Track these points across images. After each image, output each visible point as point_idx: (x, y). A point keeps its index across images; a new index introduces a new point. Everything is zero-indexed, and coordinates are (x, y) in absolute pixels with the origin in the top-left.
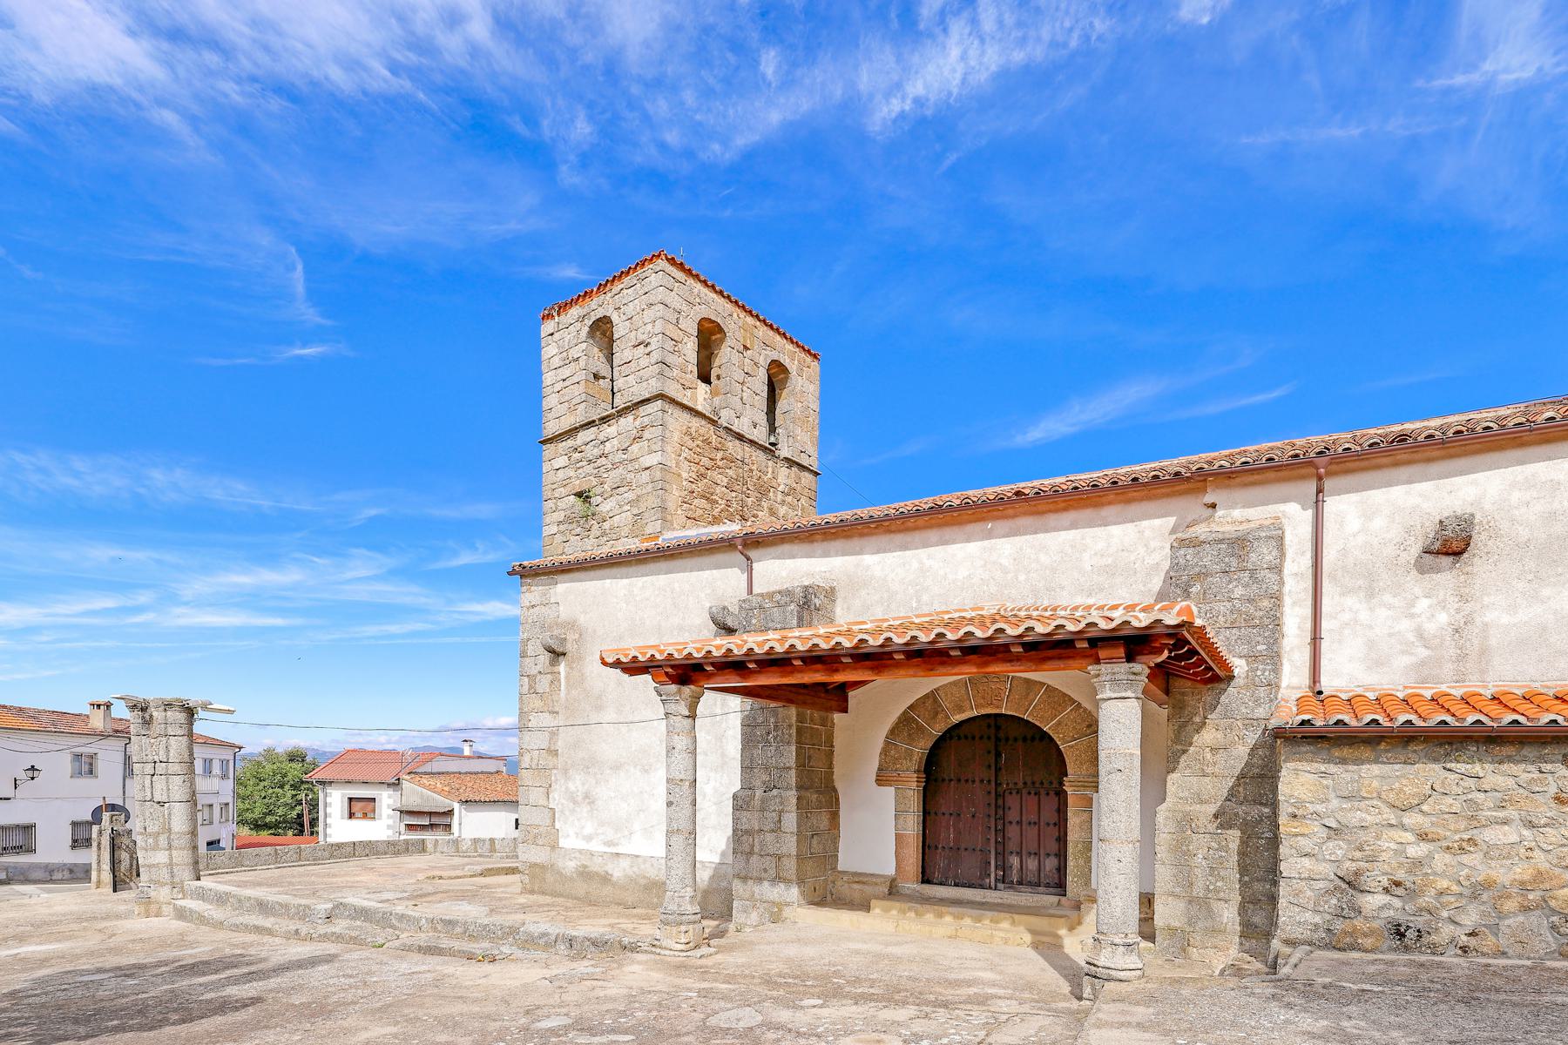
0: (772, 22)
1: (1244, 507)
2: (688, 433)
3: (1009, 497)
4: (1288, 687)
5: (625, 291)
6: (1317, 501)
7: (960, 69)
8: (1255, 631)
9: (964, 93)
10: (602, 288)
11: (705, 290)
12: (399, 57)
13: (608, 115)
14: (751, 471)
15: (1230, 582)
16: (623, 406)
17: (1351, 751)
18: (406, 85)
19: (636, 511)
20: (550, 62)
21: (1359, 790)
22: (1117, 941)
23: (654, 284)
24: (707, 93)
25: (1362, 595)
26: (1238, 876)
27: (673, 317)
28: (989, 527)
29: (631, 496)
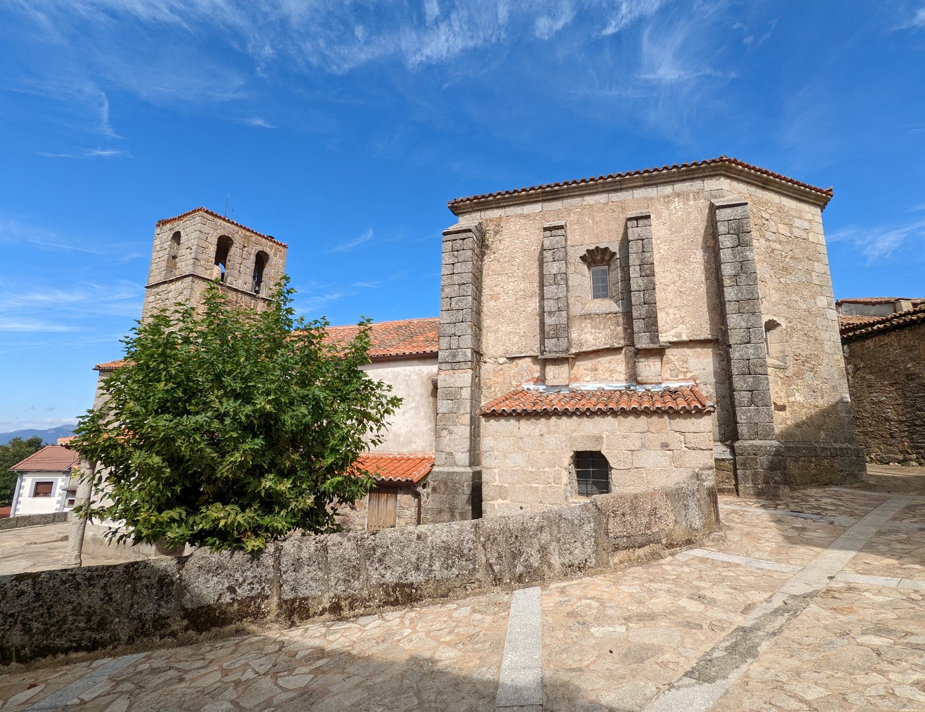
0: (360, 11)
7: (446, 45)
10: (180, 218)
18: (177, 18)
20: (254, 20)
24: (330, 42)
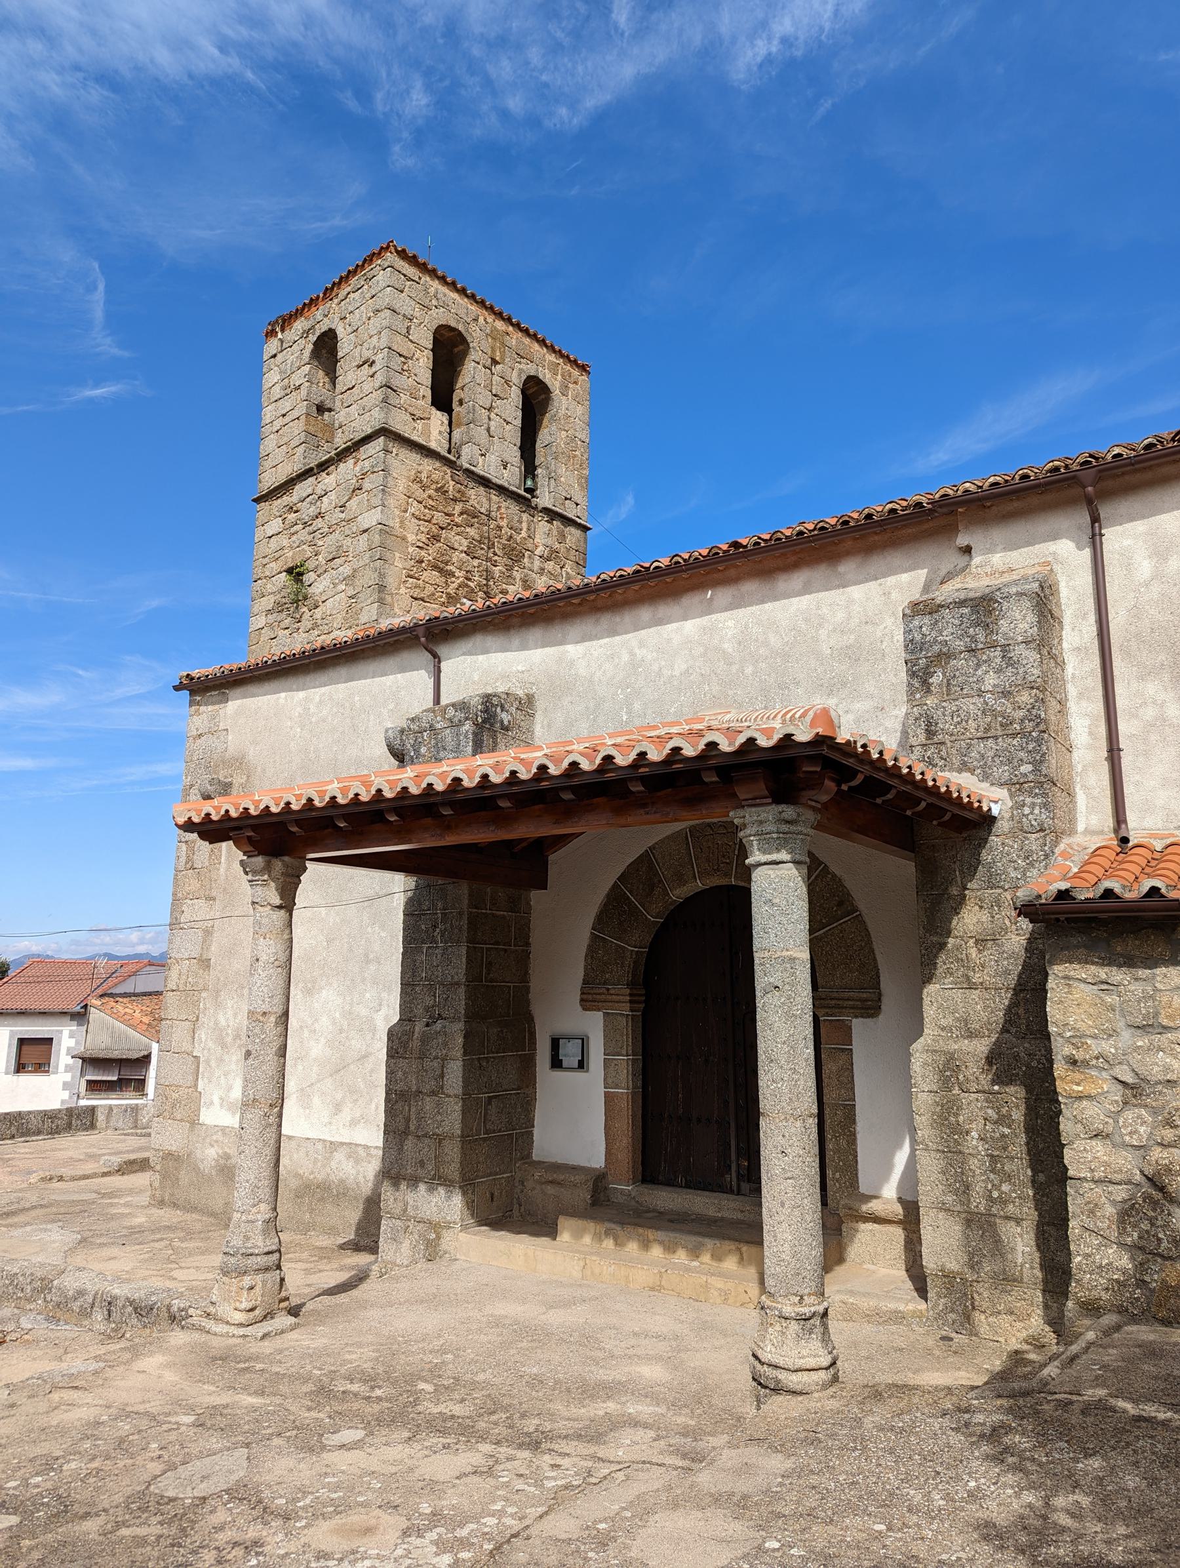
1: (1005, 549)
2: (417, 480)
3: (725, 552)
4: (1087, 831)
5: (352, 295)
6: (1094, 535)
8: (1015, 742)
9: (837, 27)
10: (328, 293)
11: (444, 289)
12: (229, 32)
13: (447, 83)
14: (500, 528)
15: (978, 666)
16: (344, 446)
17: (1137, 942)
18: (233, 63)
19: (351, 592)
21: (1156, 1014)
22: (788, 1310)
23: (382, 284)
24: (556, 48)
25: (1166, 677)
26: (1029, 1172)
27: (402, 327)
28: (709, 596)
29: (346, 570)
